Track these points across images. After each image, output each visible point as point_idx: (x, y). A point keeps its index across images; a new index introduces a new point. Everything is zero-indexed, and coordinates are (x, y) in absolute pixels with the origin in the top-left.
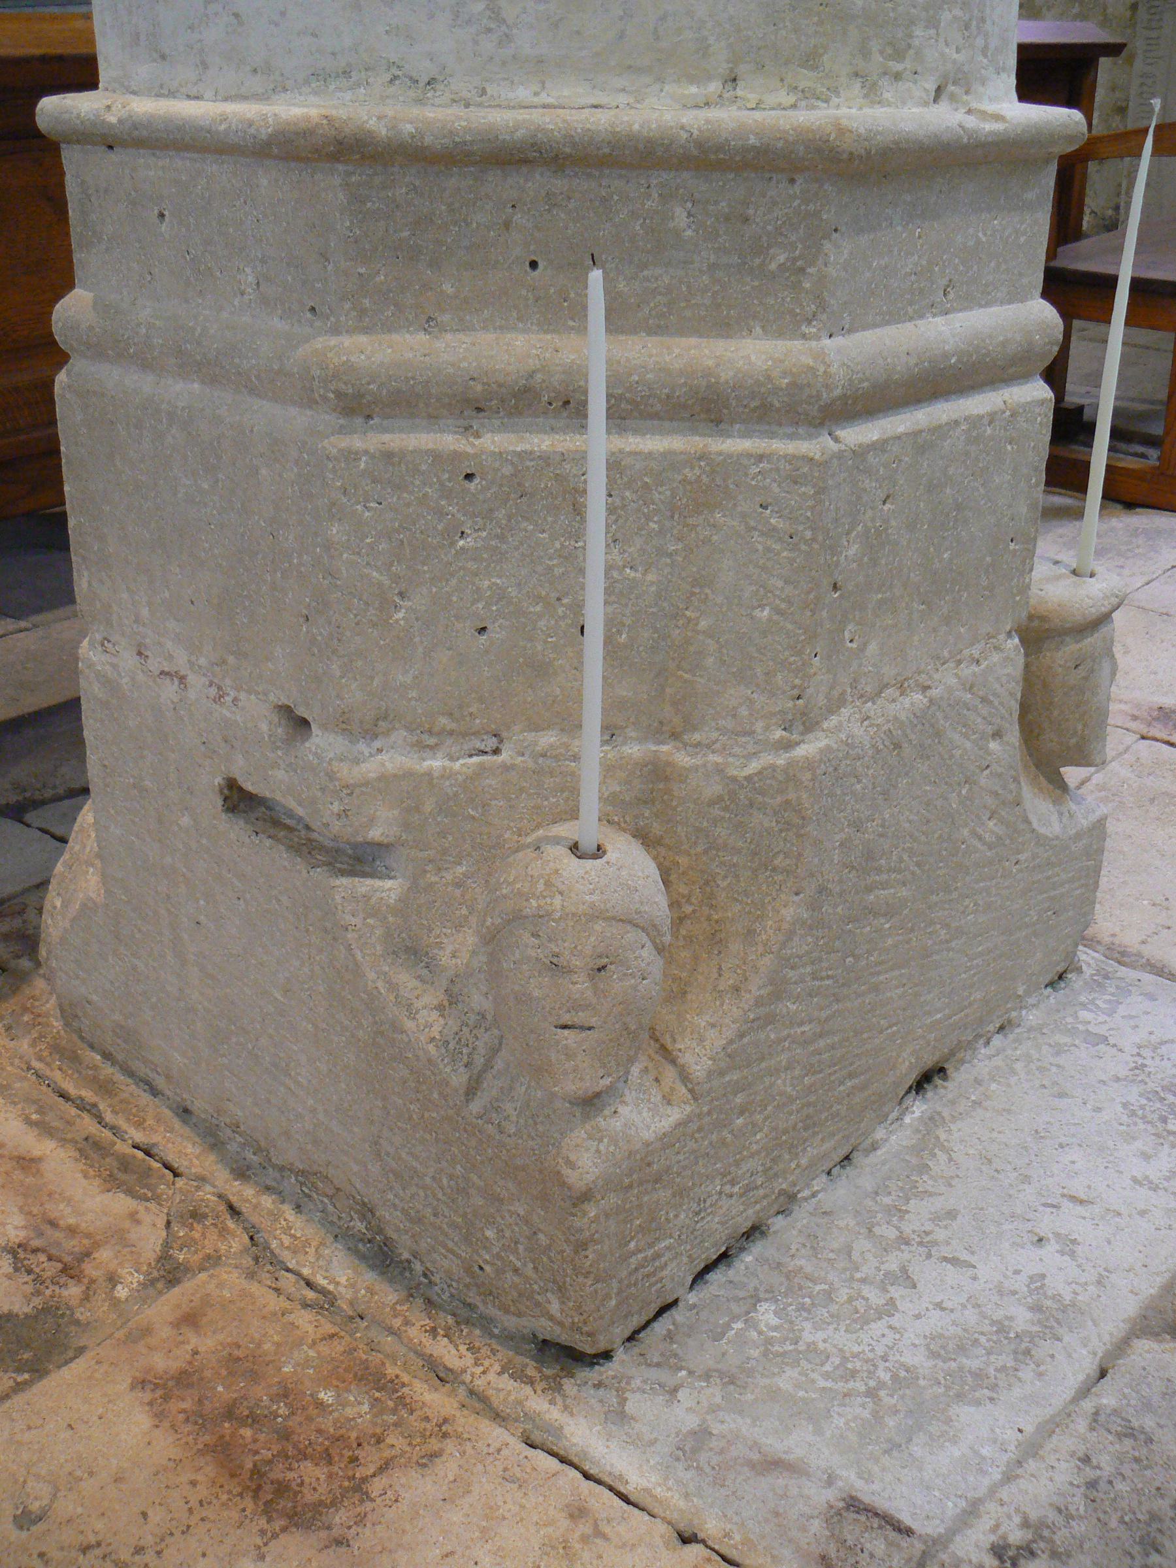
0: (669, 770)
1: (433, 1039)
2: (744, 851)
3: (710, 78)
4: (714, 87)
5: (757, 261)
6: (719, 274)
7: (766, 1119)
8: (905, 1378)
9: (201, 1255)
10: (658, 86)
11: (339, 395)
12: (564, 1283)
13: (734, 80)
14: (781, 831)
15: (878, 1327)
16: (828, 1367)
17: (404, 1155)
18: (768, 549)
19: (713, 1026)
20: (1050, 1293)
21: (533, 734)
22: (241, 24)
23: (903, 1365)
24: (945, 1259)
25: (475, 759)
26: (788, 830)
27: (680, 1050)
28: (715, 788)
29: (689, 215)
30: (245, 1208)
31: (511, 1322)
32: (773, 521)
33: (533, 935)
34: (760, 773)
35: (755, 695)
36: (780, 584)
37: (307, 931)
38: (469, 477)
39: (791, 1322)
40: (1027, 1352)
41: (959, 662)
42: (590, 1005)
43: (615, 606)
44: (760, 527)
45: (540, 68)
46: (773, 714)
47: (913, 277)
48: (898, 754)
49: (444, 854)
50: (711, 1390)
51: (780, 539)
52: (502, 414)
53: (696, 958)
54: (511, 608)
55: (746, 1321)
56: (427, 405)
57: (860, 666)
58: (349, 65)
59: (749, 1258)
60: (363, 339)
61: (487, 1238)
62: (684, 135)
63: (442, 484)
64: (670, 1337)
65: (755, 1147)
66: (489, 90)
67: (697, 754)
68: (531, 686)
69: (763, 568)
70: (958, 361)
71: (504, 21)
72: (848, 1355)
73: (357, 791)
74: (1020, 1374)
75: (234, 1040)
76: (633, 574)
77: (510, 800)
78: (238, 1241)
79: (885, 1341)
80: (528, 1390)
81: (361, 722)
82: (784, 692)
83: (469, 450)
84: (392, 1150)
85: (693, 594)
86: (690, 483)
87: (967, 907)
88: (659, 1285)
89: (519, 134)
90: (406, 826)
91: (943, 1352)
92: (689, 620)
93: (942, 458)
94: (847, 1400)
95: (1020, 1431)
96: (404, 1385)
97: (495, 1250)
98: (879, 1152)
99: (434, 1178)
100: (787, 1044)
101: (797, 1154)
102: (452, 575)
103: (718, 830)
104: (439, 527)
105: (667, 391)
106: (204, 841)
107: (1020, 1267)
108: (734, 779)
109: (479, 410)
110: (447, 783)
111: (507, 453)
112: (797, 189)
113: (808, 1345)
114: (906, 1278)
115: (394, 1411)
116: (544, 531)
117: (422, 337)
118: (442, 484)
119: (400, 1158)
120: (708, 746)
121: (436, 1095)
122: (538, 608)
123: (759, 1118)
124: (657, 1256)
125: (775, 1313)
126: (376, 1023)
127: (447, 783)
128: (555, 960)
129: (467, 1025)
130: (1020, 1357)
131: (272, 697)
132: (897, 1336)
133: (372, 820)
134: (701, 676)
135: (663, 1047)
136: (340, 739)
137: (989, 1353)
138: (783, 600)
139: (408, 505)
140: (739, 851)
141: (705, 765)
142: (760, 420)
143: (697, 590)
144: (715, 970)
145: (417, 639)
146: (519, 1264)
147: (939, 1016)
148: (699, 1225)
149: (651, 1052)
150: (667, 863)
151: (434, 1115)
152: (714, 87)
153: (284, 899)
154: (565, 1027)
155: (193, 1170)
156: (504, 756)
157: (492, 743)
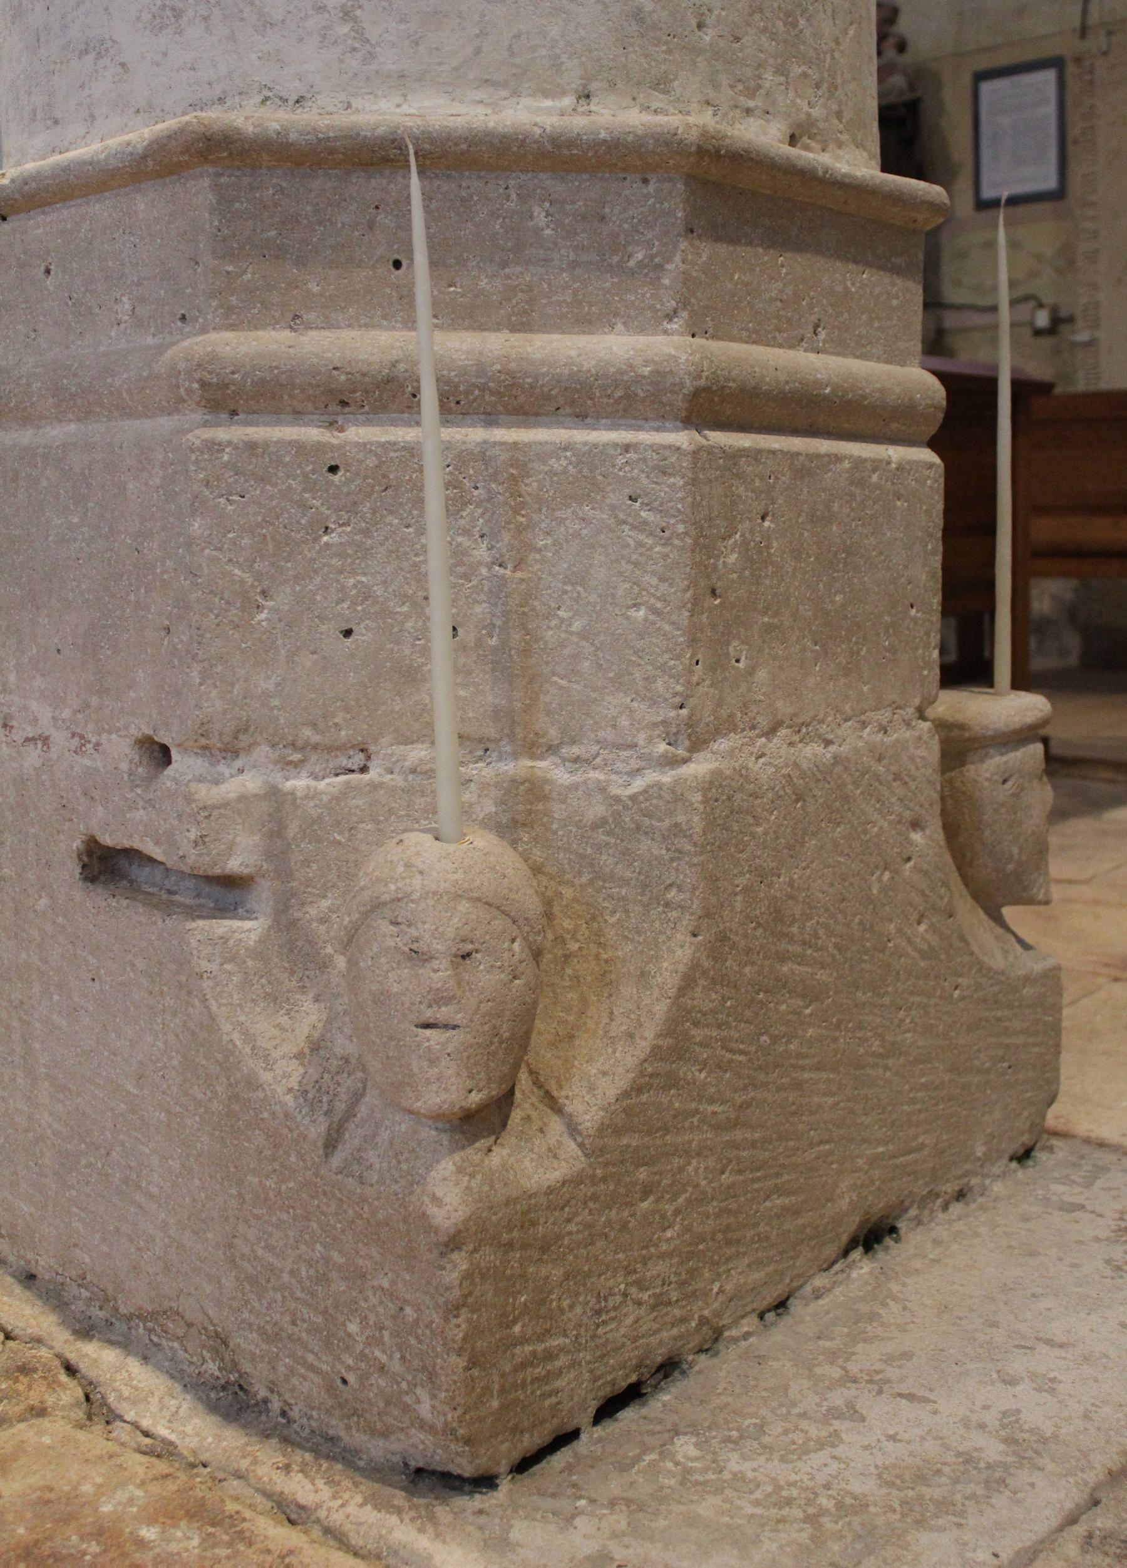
0: (547, 788)
1: (290, 1090)
2: (633, 883)
3: (564, 93)
4: (568, 101)
5: (616, 259)
6: (579, 271)
7: (677, 1212)
8: (852, 1505)
9: (22, 1407)
10: (514, 100)
11: (204, 384)
12: (434, 1366)
13: (588, 96)
14: (672, 860)
15: (823, 1456)
16: (758, 1495)
17: (260, 1252)
18: (640, 544)
19: (604, 1074)
20: (1026, 1427)
21: (402, 747)
22: (127, 71)
23: (848, 1493)
24: (900, 1395)
25: (342, 778)
26: (679, 859)
27: (567, 1097)
28: (597, 810)
29: (548, 215)
30: (83, 1366)
31: (377, 1449)
32: (643, 514)
33: (392, 923)
34: (645, 791)
35: (635, 704)
36: (654, 581)
37: (162, 993)
38: (333, 469)
39: (714, 1453)
40: (1002, 1481)
41: (864, 725)
42: (453, 997)
43: (485, 605)
44: (630, 520)
45: (402, 82)
46: (655, 725)
47: (779, 304)
48: (803, 808)
49: (308, 886)
50: (615, 1517)
51: (651, 534)
52: (367, 408)
53: (584, 1000)
54: (377, 608)
55: (661, 1454)
56: (291, 397)
57: (749, 690)
58: (224, 92)
59: (666, 1397)
60: (229, 335)
61: (349, 1335)
62: (538, 131)
63: (306, 476)
64: (569, 1468)
65: (664, 1247)
66: (354, 105)
67: (577, 770)
68: (399, 694)
69: (636, 564)
70: (833, 391)
71: (368, 41)
72: (782, 1483)
73: (215, 813)
74: (993, 1501)
75: (83, 1162)
76: (502, 571)
77: (379, 822)
78: (71, 1392)
79: (828, 1470)
80: (394, 1519)
81: (221, 734)
82: (666, 700)
83: (335, 441)
84: (246, 1250)
85: (565, 592)
86: (556, 474)
87: (902, 1021)
88: (554, 1400)
89: (379, 132)
90: (269, 855)
91: (898, 1482)
92: (562, 620)
93: (824, 490)
94: (781, 1526)
95: (996, 1555)
96: (244, 1520)
97: (359, 1347)
98: (821, 1302)
99: (292, 1273)
100: (695, 1120)
101: (719, 1275)
102: (316, 572)
103: (604, 857)
104: (303, 522)
105: (529, 380)
106: (60, 920)
107: (989, 1403)
108: (617, 799)
109: (344, 403)
110: (312, 804)
111: (371, 444)
112: (651, 188)
113: (735, 1474)
114: (853, 1413)
115: (230, 1544)
116: (408, 526)
117: (287, 333)
118: (306, 476)
119: (256, 1258)
120: (587, 761)
121: (293, 1159)
122: (405, 609)
123: (669, 1208)
124: (549, 1356)
125: (696, 1445)
126: (230, 1085)
127: (312, 804)
128: (414, 946)
129: (329, 1072)
130: (994, 1485)
131: (133, 730)
132: (843, 1466)
133: (231, 847)
134: (578, 682)
135: (547, 1093)
136: (199, 761)
137: (956, 1481)
138: (658, 599)
139: (272, 498)
140: (626, 882)
141: (585, 782)
142: (626, 413)
143: (569, 588)
144: (605, 1014)
145: (280, 642)
146: (384, 1358)
147: (881, 1149)
148: (600, 1331)
149: (534, 1099)
150: (549, 893)
151: (291, 1185)
152: (568, 101)
153: (140, 964)
154: (427, 1026)
155: (29, 1331)
156: (373, 775)
157: (358, 759)
